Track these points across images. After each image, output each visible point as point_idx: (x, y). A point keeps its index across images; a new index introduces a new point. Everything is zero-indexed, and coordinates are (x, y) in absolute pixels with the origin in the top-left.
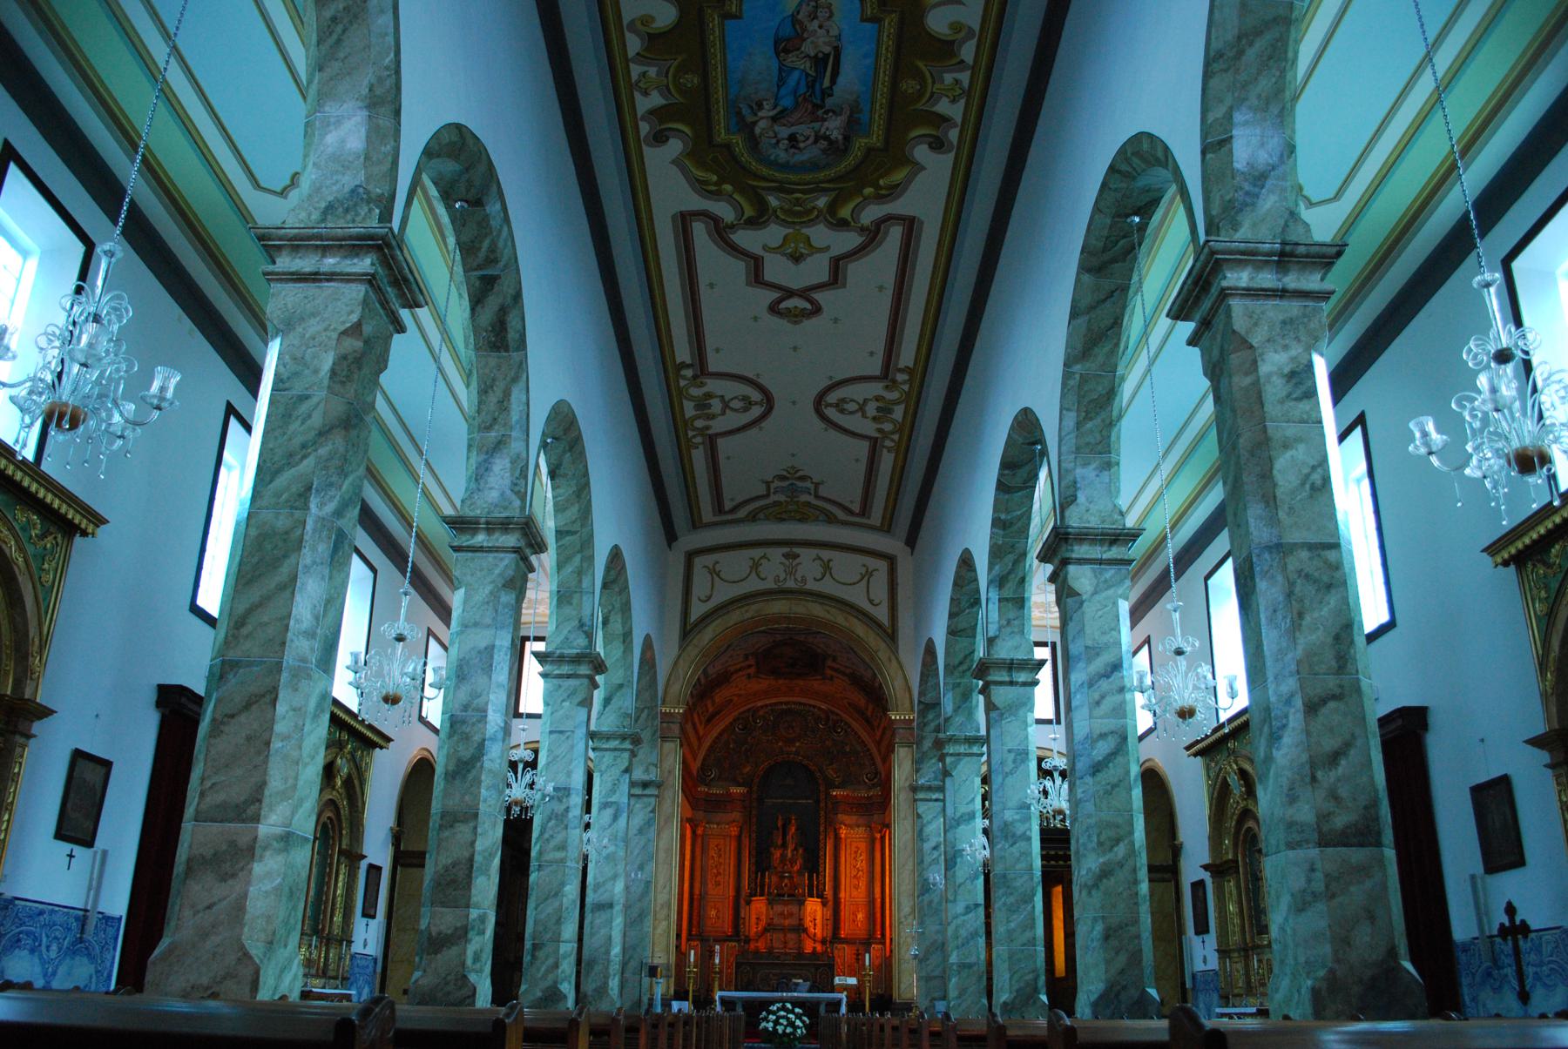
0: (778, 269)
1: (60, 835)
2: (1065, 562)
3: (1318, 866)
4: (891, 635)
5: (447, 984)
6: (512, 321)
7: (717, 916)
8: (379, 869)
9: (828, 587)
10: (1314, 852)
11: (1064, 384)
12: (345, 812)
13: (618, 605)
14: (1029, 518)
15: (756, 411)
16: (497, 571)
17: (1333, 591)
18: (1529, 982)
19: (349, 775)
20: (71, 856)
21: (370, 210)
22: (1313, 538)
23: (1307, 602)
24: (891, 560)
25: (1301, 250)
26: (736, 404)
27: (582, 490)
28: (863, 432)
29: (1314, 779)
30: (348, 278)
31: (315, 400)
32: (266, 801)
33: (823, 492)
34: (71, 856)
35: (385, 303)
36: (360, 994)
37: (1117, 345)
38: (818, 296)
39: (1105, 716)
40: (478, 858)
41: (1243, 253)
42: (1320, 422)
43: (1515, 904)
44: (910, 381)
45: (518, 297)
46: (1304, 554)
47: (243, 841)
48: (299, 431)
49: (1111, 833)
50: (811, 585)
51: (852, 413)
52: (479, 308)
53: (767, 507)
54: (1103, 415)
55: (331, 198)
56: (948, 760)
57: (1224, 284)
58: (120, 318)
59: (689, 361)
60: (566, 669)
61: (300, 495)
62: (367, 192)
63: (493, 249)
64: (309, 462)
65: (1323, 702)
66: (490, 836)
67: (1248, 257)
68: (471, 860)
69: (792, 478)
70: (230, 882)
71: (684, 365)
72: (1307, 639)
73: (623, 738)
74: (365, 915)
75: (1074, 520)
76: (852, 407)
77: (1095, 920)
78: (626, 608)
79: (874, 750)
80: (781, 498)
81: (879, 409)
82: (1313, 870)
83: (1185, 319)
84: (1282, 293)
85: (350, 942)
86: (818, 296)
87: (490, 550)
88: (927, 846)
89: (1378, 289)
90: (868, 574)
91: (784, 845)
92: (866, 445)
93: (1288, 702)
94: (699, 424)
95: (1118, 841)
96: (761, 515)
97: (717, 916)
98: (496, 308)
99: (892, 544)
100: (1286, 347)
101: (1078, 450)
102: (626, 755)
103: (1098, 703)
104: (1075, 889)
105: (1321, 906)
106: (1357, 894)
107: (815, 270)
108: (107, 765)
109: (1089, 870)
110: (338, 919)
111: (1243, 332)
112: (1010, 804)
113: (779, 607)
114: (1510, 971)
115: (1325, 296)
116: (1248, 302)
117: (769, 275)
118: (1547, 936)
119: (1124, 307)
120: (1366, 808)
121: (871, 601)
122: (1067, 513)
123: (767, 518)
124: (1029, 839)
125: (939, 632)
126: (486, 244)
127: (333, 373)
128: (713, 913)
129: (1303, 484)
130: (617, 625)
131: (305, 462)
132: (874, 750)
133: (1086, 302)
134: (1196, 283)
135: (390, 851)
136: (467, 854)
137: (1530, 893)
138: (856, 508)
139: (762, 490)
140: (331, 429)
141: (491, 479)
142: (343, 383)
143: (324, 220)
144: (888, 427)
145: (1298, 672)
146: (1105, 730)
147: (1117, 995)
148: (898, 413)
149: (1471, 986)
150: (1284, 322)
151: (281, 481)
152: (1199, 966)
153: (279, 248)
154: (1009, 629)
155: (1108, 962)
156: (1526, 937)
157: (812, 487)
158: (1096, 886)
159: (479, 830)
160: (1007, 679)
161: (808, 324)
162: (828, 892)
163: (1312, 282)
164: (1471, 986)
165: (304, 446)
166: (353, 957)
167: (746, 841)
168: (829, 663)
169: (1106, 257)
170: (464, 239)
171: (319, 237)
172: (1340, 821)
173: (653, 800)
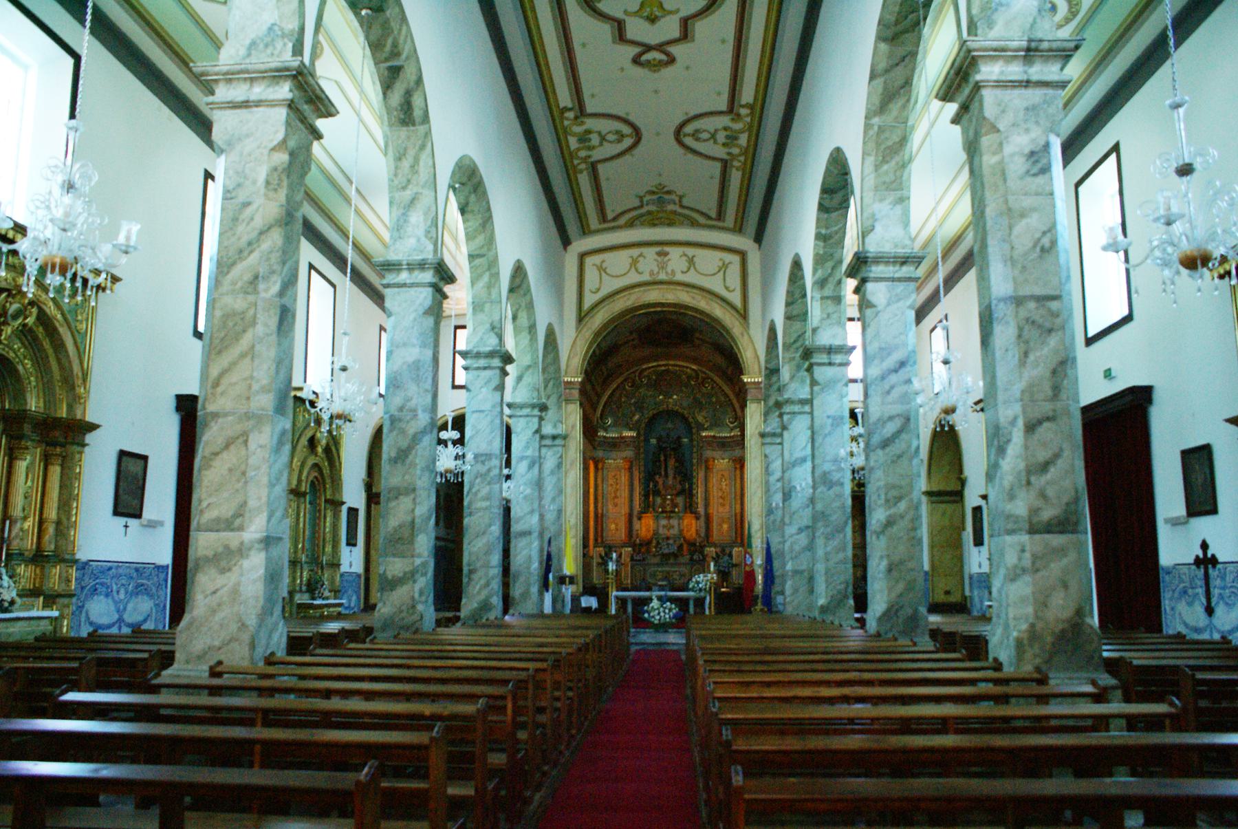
0: (637, 29)
1: (117, 512)
2: (864, 281)
3: (1028, 548)
4: (744, 315)
5: (401, 612)
6: (417, 101)
7: (616, 529)
8: (356, 510)
9: (690, 278)
10: (1025, 538)
11: (865, 132)
12: (326, 471)
13: (523, 305)
14: (844, 233)
15: (628, 142)
16: (418, 302)
17: (1053, 334)
18: (1214, 601)
19: (328, 444)
20: (126, 526)
21: (285, 45)
22: (1038, 291)
23: (1032, 344)
24: (743, 255)
25: (1045, 45)
26: (611, 137)
27: (487, 220)
28: (717, 156)
29: (1029, 483)
30: (272, 104)
31: (254, 206)
32: (247, 515)
33: (685, 202)
34: (126, 526)
35: (303, 120)
36: (350, 601)
37: (908, 101)
38: (673, 50)
39: (894, 403)
40: (417, 521)
41: (995, 50)
42: (1052, 194)
43: (1208, 541)
44: (752, 114)
45: (419, 81)
46: (1032, 305)
47: (234, 544)
48: (245, 232)
49: (894, 493)
50: (680, 277)
51: (705, 140)
52: (389, 92)
53: (642, 215)
54: (897, 158)
55: (253, 36)
56: (786, 417)
57: (978, 77)
58: (90, 180)
59: (570, 105)
60: (482, 362)
61: (251, 283)
62: (282, 29)
63: (395, 45)
64: (254, 257)
65: (1040, 422)
66: (425, 505)
67: (1000, 53)
68: (413, 522)
69: (661, 194)
70: (228, 574)
71: (566, 109)
72: (1030, 373)
73: (533, 406)
74: (348, 544)
75: (872, 247)
76: (705, 136)
77: (882, 557)
78: (530, 306)
79: (735, 401)
80: (652, 208)
81: (727, 137)
82: (1023, 551)
83: (950, 101)
84: (1027, 84)
85: (338, 565)
86: (673, 50)
87: (412, 285)
88: (772, 479)
89: (1111, 67)
90: (724, 267)
91: (666, 475)
92: (718, 165)
93: (1013, 422)
94: (583, 154)
95: (900, 499)
96: (637, 222)
97: (616, 529)
98: (402, 92)
99: (743, 242)
100: (1027, 130)
101: (876, 189)
102: (536, 420)
103: (888, 392)
104: (868, 533)
105: (1027, 578)
106: (1056, 568)
107: (669, 28)
108: (145, 458)
109: (878, 521)
110: (329, 549)
111: (992, 120)
112: (828, 458)
113: (653, 296)
114: (1201, 591)
115: (1063, 85)
116: (998, 92)
117: (630, 34)
118: (1230, 567)
119: (913, 70)
120: (1067, 504)
121: (727, 288)
122: (867, 240)
123: (642, 224)
124: (842, 484)
125: (778, 314)
126: (390, 41)
127: (268, 183)
128: (613, 526)
129: (1035, 246)
130: (523, 319)
131: (252, 256)
132: (735, 401)
133: (882, 65)
134: (957, 74)
135: (363, 495)
136: (409, 519)
137: (1224, 535)
138: (713, 214)
139: (637, 203)
140: (269, 228)
141: (409, 229)
142: (275, 190)
143: (249, 55)
144: (735, 151)
145: (1022, 400)
146: (894, 412)
147: (897, 611)
148: (743, 140)
149: (1171, 599)
150: (1027, 109)
151: (236, 271)
152: (975, 569)
153: (216, 81)
154: (829, 321)
155: (890, 590)
156: (1214, 567)
157: (677, 199)
158: (883, 532)
159: (418, 501)
160: (826, 361)
161: (667, 72)
162: (701, 509)
163: (1050, 71)
164: (1171, 599)
165: (250, 244)
166: (342, 575)
167: (636, 473)
168: (697, 335)
169: (899, 28)
170: (372, 38)
171: (247, 72)
172: (1047, 514)
173: (560, 449)
